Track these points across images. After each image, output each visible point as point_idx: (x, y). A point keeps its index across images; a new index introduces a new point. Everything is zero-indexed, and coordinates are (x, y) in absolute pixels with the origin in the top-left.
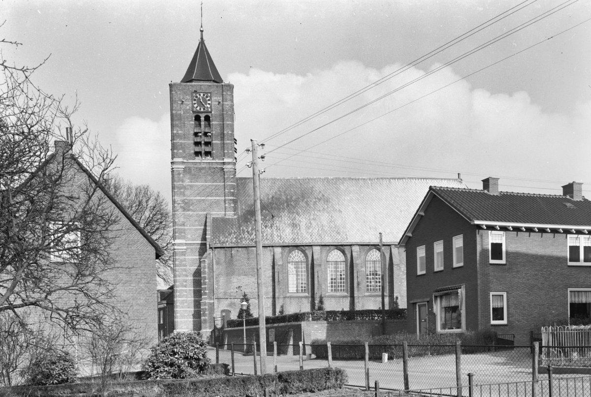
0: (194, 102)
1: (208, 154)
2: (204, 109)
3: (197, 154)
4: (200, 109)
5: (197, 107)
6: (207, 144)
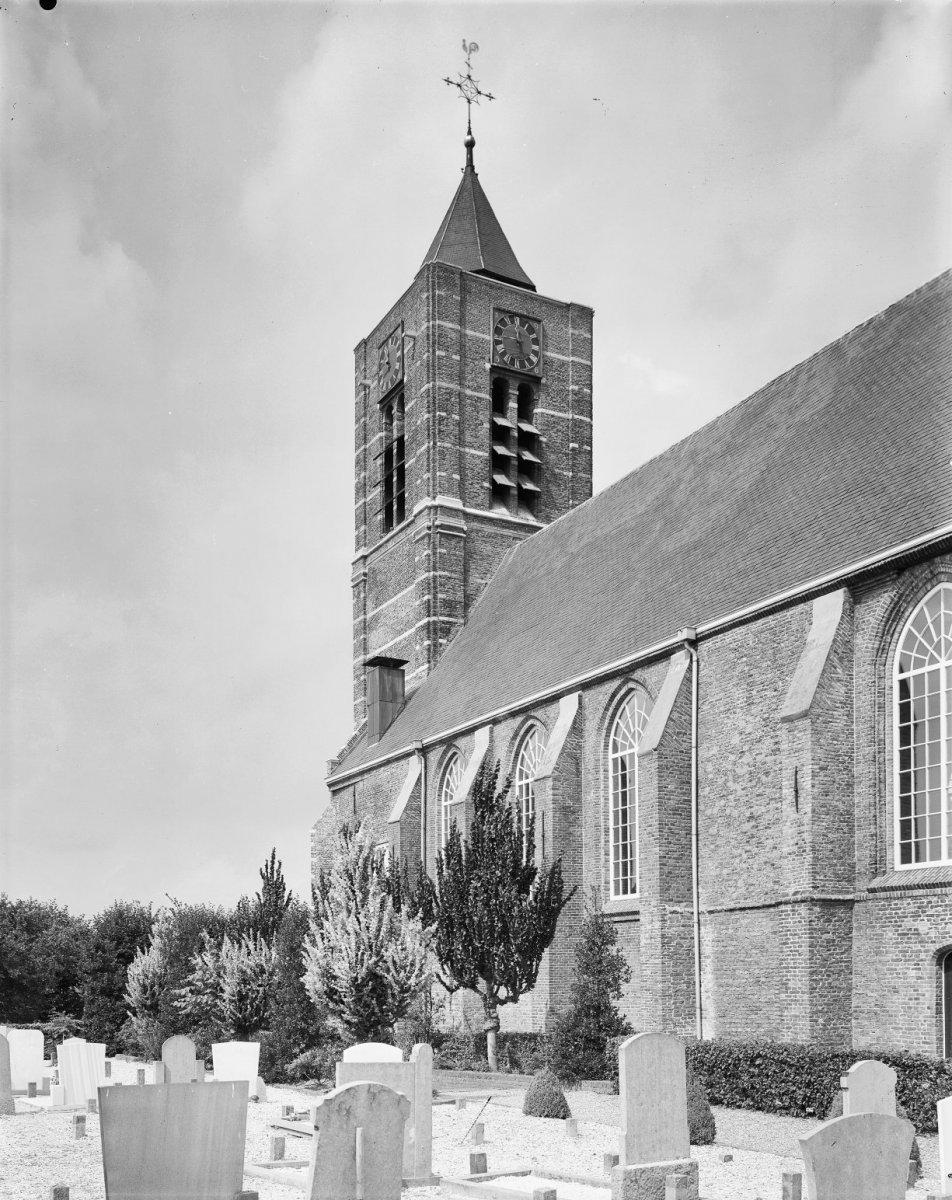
1: (527, 500)
2: (522, 365)
3: (499, 494)
6: (499, 463)
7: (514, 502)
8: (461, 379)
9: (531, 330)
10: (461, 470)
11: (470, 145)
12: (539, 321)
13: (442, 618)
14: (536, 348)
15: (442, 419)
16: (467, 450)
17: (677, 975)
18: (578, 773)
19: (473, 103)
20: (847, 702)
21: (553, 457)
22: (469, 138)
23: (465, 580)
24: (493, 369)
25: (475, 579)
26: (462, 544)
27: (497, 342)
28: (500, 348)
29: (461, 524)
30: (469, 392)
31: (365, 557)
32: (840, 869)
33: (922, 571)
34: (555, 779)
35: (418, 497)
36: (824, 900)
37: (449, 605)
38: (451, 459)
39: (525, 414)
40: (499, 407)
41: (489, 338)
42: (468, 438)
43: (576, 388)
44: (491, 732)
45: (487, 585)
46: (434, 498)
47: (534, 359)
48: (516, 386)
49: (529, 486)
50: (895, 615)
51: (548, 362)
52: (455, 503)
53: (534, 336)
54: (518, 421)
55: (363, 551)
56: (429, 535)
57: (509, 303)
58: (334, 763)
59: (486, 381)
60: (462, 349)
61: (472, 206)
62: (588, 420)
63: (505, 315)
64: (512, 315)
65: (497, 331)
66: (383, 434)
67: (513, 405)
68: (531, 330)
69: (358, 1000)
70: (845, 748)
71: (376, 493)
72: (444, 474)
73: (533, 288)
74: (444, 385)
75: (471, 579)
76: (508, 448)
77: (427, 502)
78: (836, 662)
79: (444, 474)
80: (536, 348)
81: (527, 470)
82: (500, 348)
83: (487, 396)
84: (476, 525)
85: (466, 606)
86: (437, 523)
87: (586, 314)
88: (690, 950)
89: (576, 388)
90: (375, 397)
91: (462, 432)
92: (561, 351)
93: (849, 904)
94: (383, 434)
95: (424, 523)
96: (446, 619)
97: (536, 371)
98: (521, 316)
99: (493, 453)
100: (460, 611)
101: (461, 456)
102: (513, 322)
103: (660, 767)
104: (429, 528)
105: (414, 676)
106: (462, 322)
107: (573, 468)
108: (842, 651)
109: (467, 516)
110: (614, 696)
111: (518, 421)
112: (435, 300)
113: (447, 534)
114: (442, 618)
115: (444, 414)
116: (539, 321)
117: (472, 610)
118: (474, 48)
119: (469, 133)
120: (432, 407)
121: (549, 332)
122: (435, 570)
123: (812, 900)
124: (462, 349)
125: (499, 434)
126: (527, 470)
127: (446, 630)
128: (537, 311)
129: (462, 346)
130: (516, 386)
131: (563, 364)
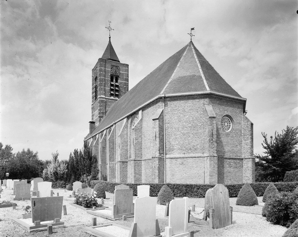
1: (117, 96)
2: (116, 74)
3: (112, 95)
4: (114, 74)
6: (112, 90)
7: (114, 96)
8: (105, 77)
9: (117, 68)
10: (105, 91)
11: (110, 38)
12: (119, 67)
13: (101, 115)
14: (118, 71)
15: (101, 83)
16: (106, 88)
17: (112, 172)
18: (106, 142)
19: (110, 31)
20: (127, 134)
21: (121, 88)
22: (109, 36)
23: (106, 109)
24: (111, 75)
25: (107, 109)
26: (105, 103)
27: (111, 70)
28: (112, 71)
29: (105, 100)
30: (106, 79)
31: (93, 104)
32: (125, 157)
33: (133, 116)
34: (102, 143)
35: (98, 96)
36: (122, 162)
37: (103, 113)
38: (103, 89)
39: (117, 81)
40: (112, 80)
41: (110, 70)
42: (106, 86)
43: (125, 77)
44: (99, 135)
45: (109, 109)
46: (100, 96)
47: (118, 73)
48: (114, 77)
50: (132, 122)
51: (120, 73)
52: (104, 97)
53: (118, 69)
54: (115, 83)
55: (93, 103)
56: (99, 102)
57: (114, 64)
58: (85, 138)
59: (109, 77)
60: (105, 72)
61: (110, 49)
62: (127, 82)
63: (112, 66)
64: (114, 66)
65: (111, 69)
66: (95, 84)
67: (114, 80)
68: (117, 68)
69: (54, 175)
70: (126, 140)
71: (94, 94)
72: (102, 92)
73: (119, 62)
74: (102, 77)
75: (107, 109)
76: (113, 87)
77: (99, 96)
78: (125, 128)
79: (102, 92)
80: (118, 71)
81: (117, 91)
82: (112, 71)
83: (109, 79)
84: (108, 100)
85: (106, 113)
86: (101, 100)
87: (128, 65)
88: (114, 168)
89: (125, 77)
90: (94, 78)
91: (105, 85)
92: (123, 71)
93: (127, 162)
94: (95, 84)
95: (99, 100)
96: (102, 115)
97: (118, 75)
98: (116, 66)
99: (111, 88)
100: (104, 114)
101: (105, 89)
102: (114, 67)
103: (109, 142)
104: (99, 101)
105: (97, 124)
106: (105, 67)
107: (125, 90)
108: (126, 127)
109: (106, 98)
110: (109, 130)
111: (115, 83)
112: (101, 64)
113: (102, 101)
114: (101, 115)
115: (102, 82)
116: (119, 67)
117: (107, 114)
118: (111, 22)
119: (110, 36)
120: (100, 81)
121: (121, 68)
122: (100, 107)
123: (120, 162)
124: (105, 72)
125: (112, 85)
126: (117, 91)
127: (102, 117)
128: (118, 65)
129: (105, 71)
130: (114, 77)
131: (123, 73)
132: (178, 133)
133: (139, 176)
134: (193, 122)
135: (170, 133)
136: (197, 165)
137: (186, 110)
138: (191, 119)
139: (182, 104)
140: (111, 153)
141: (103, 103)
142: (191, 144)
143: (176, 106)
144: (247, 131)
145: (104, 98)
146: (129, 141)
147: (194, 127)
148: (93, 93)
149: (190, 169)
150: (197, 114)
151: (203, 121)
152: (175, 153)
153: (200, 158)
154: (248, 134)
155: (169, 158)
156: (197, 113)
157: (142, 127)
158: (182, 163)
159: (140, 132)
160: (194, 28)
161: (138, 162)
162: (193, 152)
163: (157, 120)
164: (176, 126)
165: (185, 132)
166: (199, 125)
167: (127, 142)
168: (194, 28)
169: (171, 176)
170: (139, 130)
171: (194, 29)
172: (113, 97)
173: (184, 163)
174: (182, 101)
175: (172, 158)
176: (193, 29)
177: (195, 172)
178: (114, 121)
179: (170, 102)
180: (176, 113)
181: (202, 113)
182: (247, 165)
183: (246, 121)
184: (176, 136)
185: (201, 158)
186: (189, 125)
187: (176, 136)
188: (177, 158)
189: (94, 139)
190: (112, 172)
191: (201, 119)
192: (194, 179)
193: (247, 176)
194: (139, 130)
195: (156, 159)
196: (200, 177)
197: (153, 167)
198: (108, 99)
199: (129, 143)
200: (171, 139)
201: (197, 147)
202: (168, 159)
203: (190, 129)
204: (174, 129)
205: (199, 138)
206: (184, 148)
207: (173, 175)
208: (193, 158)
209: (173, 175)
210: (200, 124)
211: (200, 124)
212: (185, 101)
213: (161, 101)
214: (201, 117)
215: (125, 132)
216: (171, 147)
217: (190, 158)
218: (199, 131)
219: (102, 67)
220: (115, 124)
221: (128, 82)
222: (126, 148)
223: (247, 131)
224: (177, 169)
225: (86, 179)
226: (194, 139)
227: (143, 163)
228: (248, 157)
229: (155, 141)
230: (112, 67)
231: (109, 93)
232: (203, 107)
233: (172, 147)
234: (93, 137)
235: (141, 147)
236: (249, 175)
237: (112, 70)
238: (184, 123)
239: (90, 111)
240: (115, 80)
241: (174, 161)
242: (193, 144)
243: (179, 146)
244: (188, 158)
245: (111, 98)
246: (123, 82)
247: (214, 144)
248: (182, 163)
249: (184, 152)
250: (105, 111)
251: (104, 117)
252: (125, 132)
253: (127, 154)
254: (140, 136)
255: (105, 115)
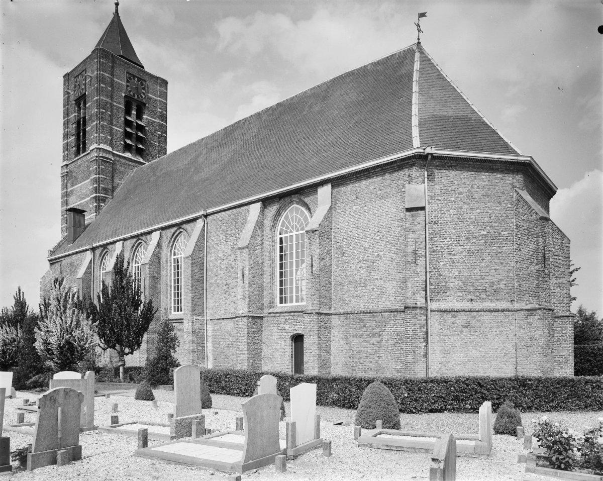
0: (127, 84)
1: (140, 152)
2: (138, 97)
3: (127, 148)
4: (134, 95)
5: (130, 91)
6: (127, 135)
8: (112, 98)
9: (142, 84)
10: (111, 135)
12: (146, 81)
13: (102, 195)
14: (144, 91)
16: (114, 127)
17: (198, 343)
18: (159, 263)
20: (261, 244)
21: (151, 136)
23: (113, 181)
24: (125, 96)
25: (117, 181)
26: (111, 165)
29: (111, 157)
31: (67, 165)
33: (288, 199)
34: (150, 265)
36: (252, 316)
37: (105, 190)
39: (139, 117)
40: (128, 112)
42: (114, 122)
44: (123, 243)
45: (122, 183)
46: (99, 145)
47: (143, 96)
49: (140, 146)
50: (278, 214)
52: (109, 149)
55: (66, 163)
58: (51, 251)
59: (122, 101)
61: (116, 31)
64: (134, 77)
65: (128, 81)
67: (134, 112)
68: (142, 84)
71: (72, 139)
73: (143, 68)
80: (144, 91)
81: (140, 140)
84: (117, 158)
85: (113, 191)
88: (203, 334)
91: (112, 120)
92: (154, 95)
93: (262, 318)
95: (94, 154)
96: (104, 195)
98: (138, 78)
99: (125, 130)
101: (111, 129)
102: (134, 79)
104: (97, 157)
105: (89, 217)
106: (112, 74)
107: (159, 142)
108: (260, 225)
109: (114, 154)
113: (105, 161)
114: (102, 195)
115: (104, 111)
116: (146, 81)
121: (150, 86)
123: (248, 316)
125: (128, 123)
127: (104, 200)
130: (135, 104)
132: (459, 249)
133: (327, 356)
134: (491, 226)
135: (439, 248)
136: (500, 329)
137: (475, 196)
138: (486, 219)
139: (466, 180)
140: (197, 294)
141: (107, 164)
142: (487, 278)
143: (452, 181)
144: (561, 258)
145: (109, 151)
146: (267, 262)
147: (493, 238)
148: (66, 136)
149: (485, 339)
150: (498, 208)
151: (511, 225)
152: (451, 298)
153: (507, 312)
154: (563, 265)
155: (438, 311)
156: (498, 205)
157: (332, 229)
158: (469, 324)
159: (327, 241)
160: (425, 13)
161: (326, 318)
162: (490, 298)
163: (420, 212)
164: (454, 231)
165: (473, 248)
166: (503, 233)
167: (260, 266)
168: (425, 13)
169: (442, 356)
170: (326, 236)
171: (426, 15)
172: (131, 154)
173: (473, 322)
174: (466, 173)
175: (444, 311)
176: (422, 15)
177: (497, 345)
178: (205, 209)
179: (439, 171)
180: (453, 199)
181: (509, 206)
182: (561, 331)
183: (558, 236)
184: (453, 257)
185: (509, 313)
186: (482, 232)
187: (453, 257)
188: (456, 311)
189: (100, 255)
190: (198, 343)
191: (508, 220)
192: (494, 363)
193: (561, 354)
194: (326, 236)
195: (418, 311)
196: (506, 358)
197: (411, 332)
198: (118, 155)
199: (266, 269)
200: (442, 263)
201: (498, 286)
202: (436, 313)
203: (483, 241)
204: (448, 240)
205: (503, 265)
206: (472, 288)
207: (447, 353)
208: (493, 311)
209: (447, 353)
210: (506, 233)
211: (506, 233)
212: (473, 173)
213: (419, 164)
214: (507, 216)
215: (258, 240)
216: (441, 282)
217: (485, 311)
218: (504, 248)
219: (105, 72)
220: (206, 216)
221: (166, 123)
222: (259, 282)
223: (561, 258)
224: (456, 338)
225: (120, 363)
226: (492, 268)
227: (335, 321)
228: (564, 314)
229: (413, 265)
230: (130, 78)
231: (122, 143)
232: (511, 194)
233: (443, 284)
234: (93, 249)
235: (330, 280)
236: (565, 353)
237: (129, 84)
238: (472, 227)
239: (58, 182)
240: (137, 111)
241: (449, 317)
242: (490, 278)
243: (460, 282)
244: (481, 313)
245: (126, 156)
246: (154, 120)
247: (546, 281)
248: (469, 324)
249: (470, 297)
250: (112, 185)
251: (110, 202)
252: (258, 240)
253: (261, 297)
254: (328, 250)
255: (112, 195)
